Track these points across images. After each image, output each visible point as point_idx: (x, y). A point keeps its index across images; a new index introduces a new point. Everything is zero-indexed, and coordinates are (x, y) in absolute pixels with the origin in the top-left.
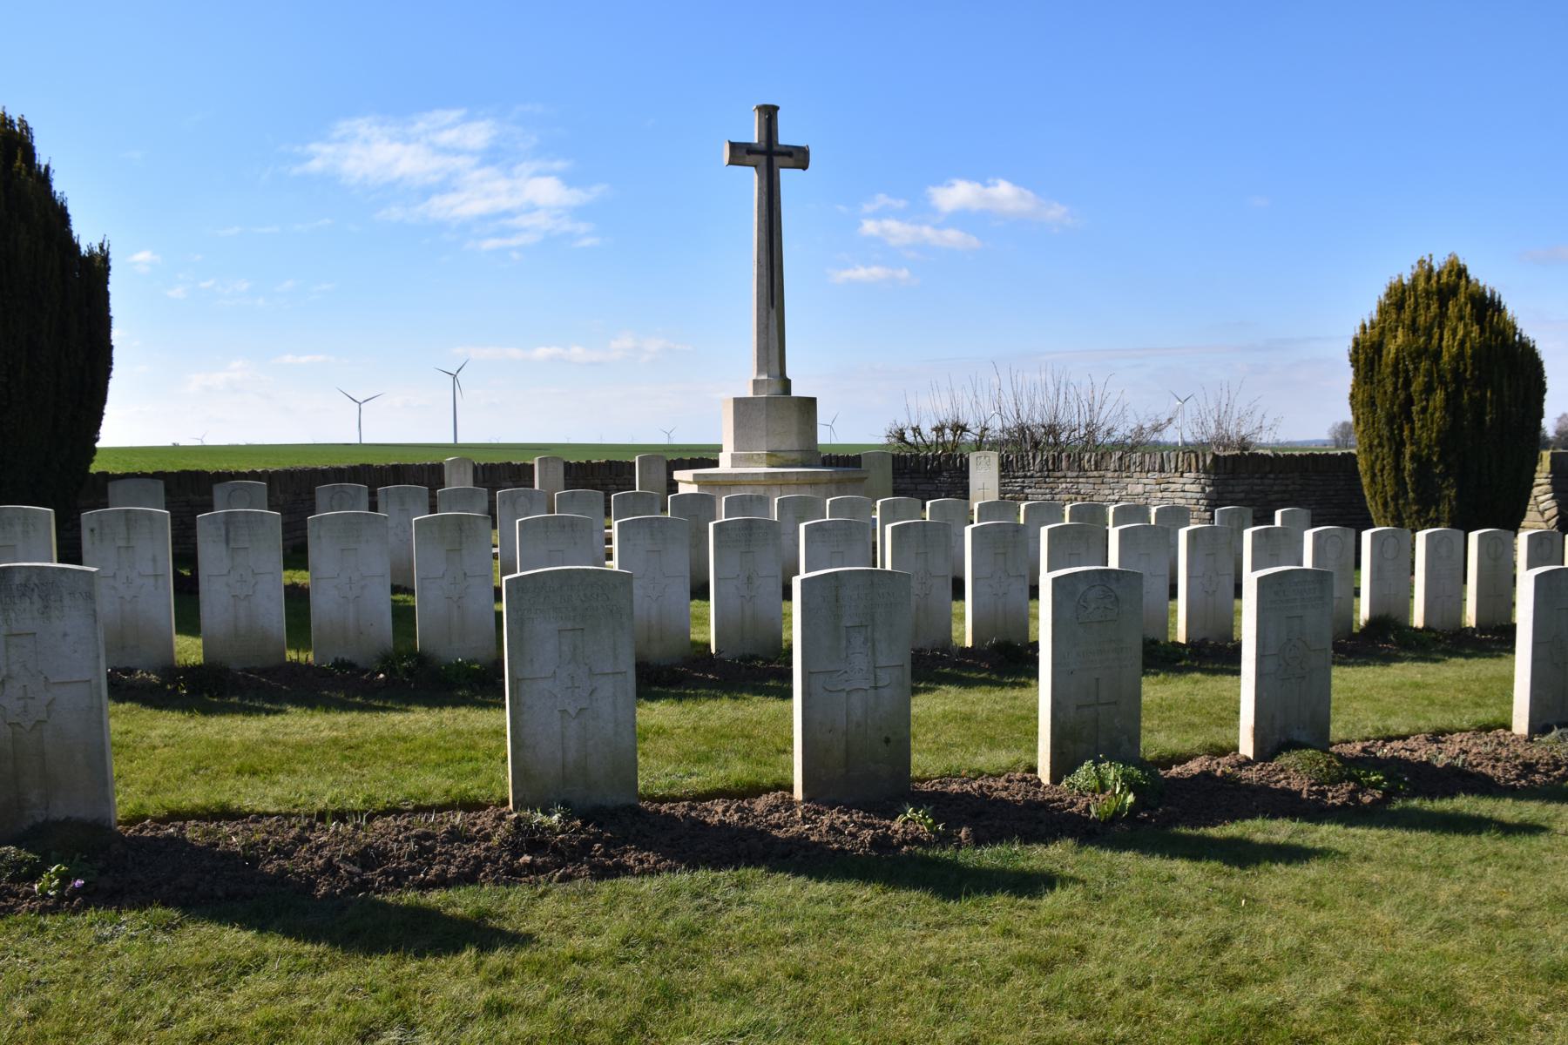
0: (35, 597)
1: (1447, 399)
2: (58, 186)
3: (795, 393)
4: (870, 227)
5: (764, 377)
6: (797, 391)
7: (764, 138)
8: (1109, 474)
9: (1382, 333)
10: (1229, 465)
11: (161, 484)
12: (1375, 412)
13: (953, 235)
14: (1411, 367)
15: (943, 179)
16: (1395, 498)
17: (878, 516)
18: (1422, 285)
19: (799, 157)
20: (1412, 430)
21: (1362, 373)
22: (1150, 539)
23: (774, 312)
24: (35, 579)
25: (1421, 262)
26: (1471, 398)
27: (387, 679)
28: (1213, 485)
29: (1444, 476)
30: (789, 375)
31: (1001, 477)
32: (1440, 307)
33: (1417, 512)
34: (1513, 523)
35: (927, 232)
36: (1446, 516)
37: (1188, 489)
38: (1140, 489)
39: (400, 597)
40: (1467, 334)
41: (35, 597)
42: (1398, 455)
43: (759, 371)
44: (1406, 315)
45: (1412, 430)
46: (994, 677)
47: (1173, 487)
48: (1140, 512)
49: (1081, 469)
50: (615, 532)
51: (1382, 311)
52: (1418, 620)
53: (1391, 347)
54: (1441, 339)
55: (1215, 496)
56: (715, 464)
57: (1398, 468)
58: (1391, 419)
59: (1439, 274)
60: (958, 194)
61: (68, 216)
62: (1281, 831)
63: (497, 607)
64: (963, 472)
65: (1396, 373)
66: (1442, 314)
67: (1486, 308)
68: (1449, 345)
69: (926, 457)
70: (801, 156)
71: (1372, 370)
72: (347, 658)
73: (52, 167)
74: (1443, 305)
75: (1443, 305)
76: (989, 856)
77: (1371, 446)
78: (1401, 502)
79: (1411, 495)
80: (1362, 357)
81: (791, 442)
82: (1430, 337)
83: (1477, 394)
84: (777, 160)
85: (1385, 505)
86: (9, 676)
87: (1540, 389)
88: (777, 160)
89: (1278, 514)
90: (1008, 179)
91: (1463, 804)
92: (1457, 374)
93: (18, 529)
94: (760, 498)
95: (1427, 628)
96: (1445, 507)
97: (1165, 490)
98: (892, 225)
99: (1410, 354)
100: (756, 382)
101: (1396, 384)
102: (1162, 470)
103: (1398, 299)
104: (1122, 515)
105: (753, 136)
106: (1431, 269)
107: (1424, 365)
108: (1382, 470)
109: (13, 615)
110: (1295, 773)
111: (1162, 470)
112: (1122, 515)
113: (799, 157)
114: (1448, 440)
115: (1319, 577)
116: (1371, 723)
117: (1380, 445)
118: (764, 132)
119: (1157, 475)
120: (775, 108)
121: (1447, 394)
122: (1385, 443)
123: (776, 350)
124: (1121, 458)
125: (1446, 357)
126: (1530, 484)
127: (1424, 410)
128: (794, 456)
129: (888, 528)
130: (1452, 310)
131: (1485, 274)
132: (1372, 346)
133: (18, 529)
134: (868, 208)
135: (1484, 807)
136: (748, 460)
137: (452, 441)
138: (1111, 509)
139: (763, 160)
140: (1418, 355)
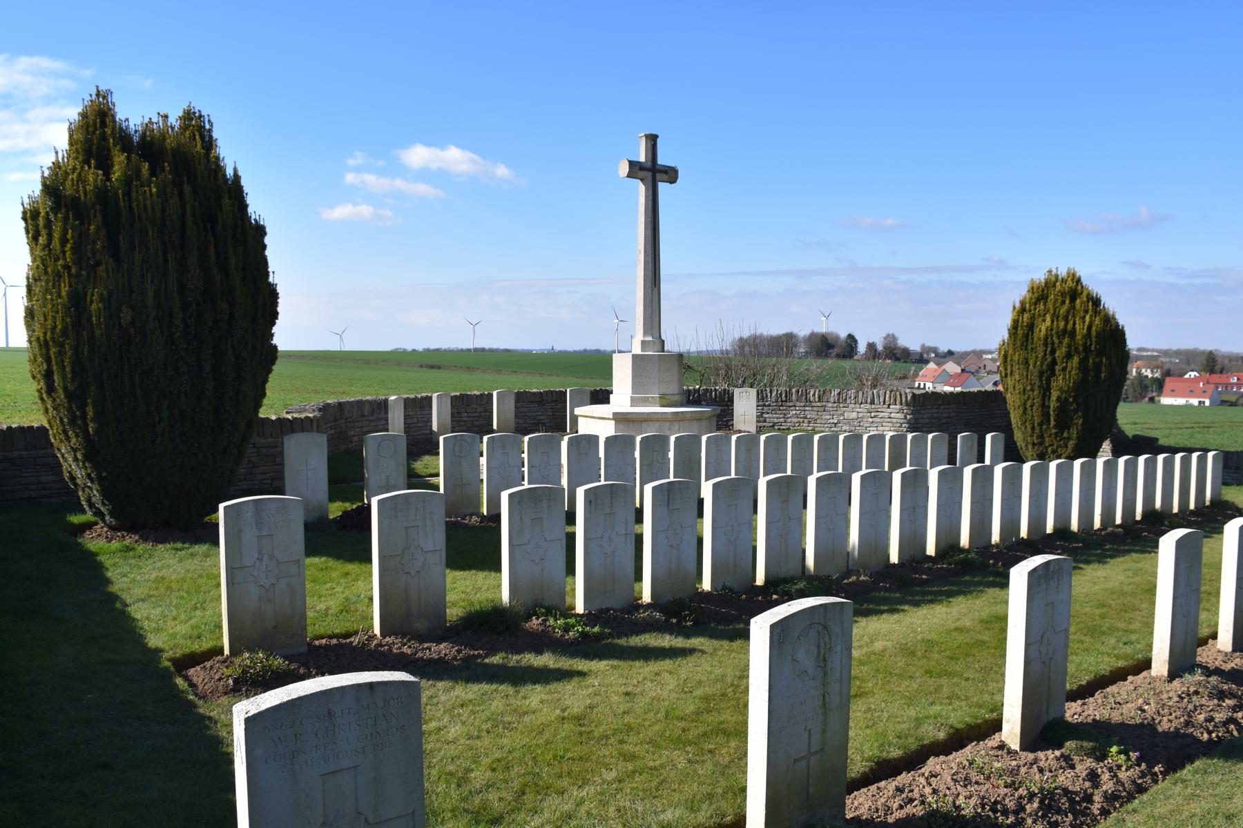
4: (350, 178)
5: (650, 339)
13: (422, 189)
15: (407, 143)
16: (1041, 425)
19: (671, 175)
21: (1019, 343)
23: (656, 290)
25: (1050, 272)
33: (1056, 434)
35: (399, 184)
38: (854, 415)
43: (645, 334)
53: (1043, 327)
54: (1074, 324)
57: (1044, 406)
58: (1041, 374)
60: (418, 155)
62: (546, 660)
63: (569, 529)
65: (1046, 345)
66: (1073, 307)
68: (1081, 329)
75: (1073, 300)
79: (1052, 423)
81: (673, 388)
84: (659, 176)
85: (1033, 428)
88: (659, 176)
90: (459, 145)
92: (1086, 348)
93: (545, 504)
98: (370, 178)
100: (643, 342)
102: (872, 402)
106: (1057, 276)
111: (872, 402)
113: (671, 175)
117: (1032, 390)
119: (868, 406)
122: (1036, 387)
125: (1078, 337)
127: (1064, 369)
131: (1092, 284)
133: (545, 504)
134: (351, 162)
136: (645, 402)
137: (4, 345)
139: (649, 175)
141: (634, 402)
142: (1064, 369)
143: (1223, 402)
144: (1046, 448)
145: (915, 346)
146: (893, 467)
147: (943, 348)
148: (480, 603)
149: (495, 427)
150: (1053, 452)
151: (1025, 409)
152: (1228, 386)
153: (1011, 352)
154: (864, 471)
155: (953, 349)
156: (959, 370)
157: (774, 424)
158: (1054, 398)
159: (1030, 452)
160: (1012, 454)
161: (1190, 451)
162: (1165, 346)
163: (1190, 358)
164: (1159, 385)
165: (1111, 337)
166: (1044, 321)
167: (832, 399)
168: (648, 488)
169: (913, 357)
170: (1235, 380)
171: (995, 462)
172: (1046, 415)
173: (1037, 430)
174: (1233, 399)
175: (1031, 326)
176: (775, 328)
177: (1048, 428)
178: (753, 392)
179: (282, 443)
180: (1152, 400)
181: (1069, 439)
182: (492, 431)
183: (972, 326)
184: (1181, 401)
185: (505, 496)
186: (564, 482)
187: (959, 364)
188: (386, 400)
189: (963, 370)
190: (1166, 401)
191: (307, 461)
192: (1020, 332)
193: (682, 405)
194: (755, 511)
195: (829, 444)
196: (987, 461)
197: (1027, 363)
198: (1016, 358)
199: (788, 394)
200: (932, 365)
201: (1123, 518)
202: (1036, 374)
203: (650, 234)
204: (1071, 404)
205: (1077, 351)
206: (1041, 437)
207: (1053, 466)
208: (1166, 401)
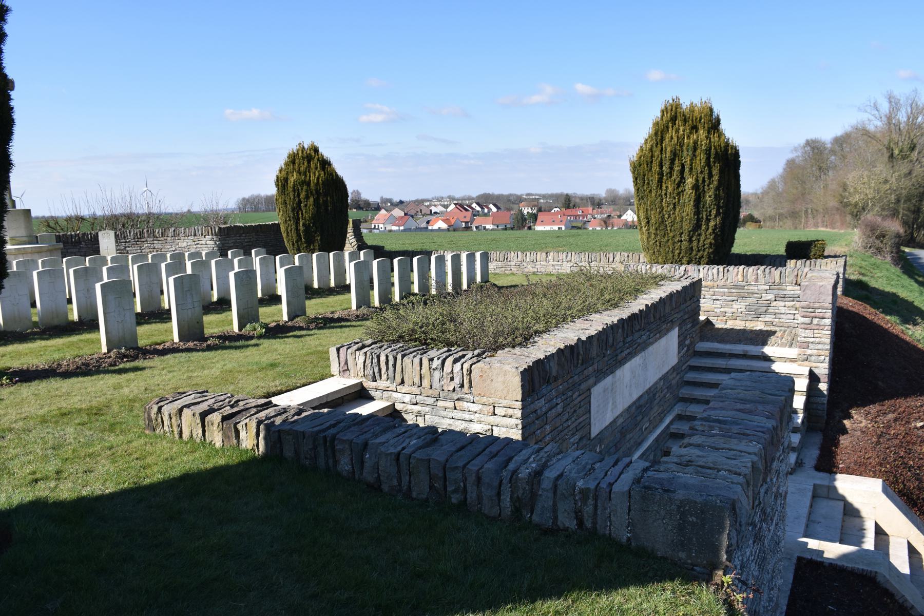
1: (314, 201)
9: (287, 174)
16: (297, 242)
17: (64, 266)
18: (300, 154)
22: (201, 265)
31: (116, 242)
34: (341, 248)
37: (207, 244)
38: (185, 244)
40: (319, 175)
42: (297, 224)
44: (296, 166)
48: (198, 254)
49: (154, 236)
50: (189, 265)
51: (287, 164)
52: (316, 286)
53: (292, 180)
57: (297, 230)
58: (293, 210)
65: (294, 191)
66: (309, 166)
67: (325, 164)
68: (313, 179)
74: (309, 162)
75: (309, 162)
76: (233, 344)
85: (293, 245)
87: (345, 186)
89: (229, 252)
91: (343, 324)
94: (33, 260)
95: (319, 288)
96: (317, 244)
102: (195, 235)
103: (293, 159)
104: (191, 256)
107: (305, 187)
110: (299, 321)
111: (195, 235)
112: (191, 256)
114: (315, 218)
115: (300, 267)
116: (314, 312)
125: (312, 185)
126: (346, 232)
127: (306, 206)
128: (25, 239)
129: (71, 271)
130: (312, 165)
131: (326, 152)
135: (349, 324)
138: (187, 254)
140: (303, 183)
143: (573, 227)
145: (374, 198)
147: (396, 199)
148: (906, 600)
152: (576, 216)
155: (403, 200)
156: (403, 214)
161: (391, 255)
162: (543, 192)
163: (556, 197)
164: (534, 217)
165: (336, 185)
170: (580, 213)
172: (298, 235)
174: (580, 225)
175: (286, 180)
178: (112, 233)
180: (530, 228)
183: (249, 179)
184: (548, 228)
187: (403, 210)
189: (406, 214)
190: (539, 228)
196: (230, 257)
199: (142, 233)
200: (383, 212)
208: (539, 228)
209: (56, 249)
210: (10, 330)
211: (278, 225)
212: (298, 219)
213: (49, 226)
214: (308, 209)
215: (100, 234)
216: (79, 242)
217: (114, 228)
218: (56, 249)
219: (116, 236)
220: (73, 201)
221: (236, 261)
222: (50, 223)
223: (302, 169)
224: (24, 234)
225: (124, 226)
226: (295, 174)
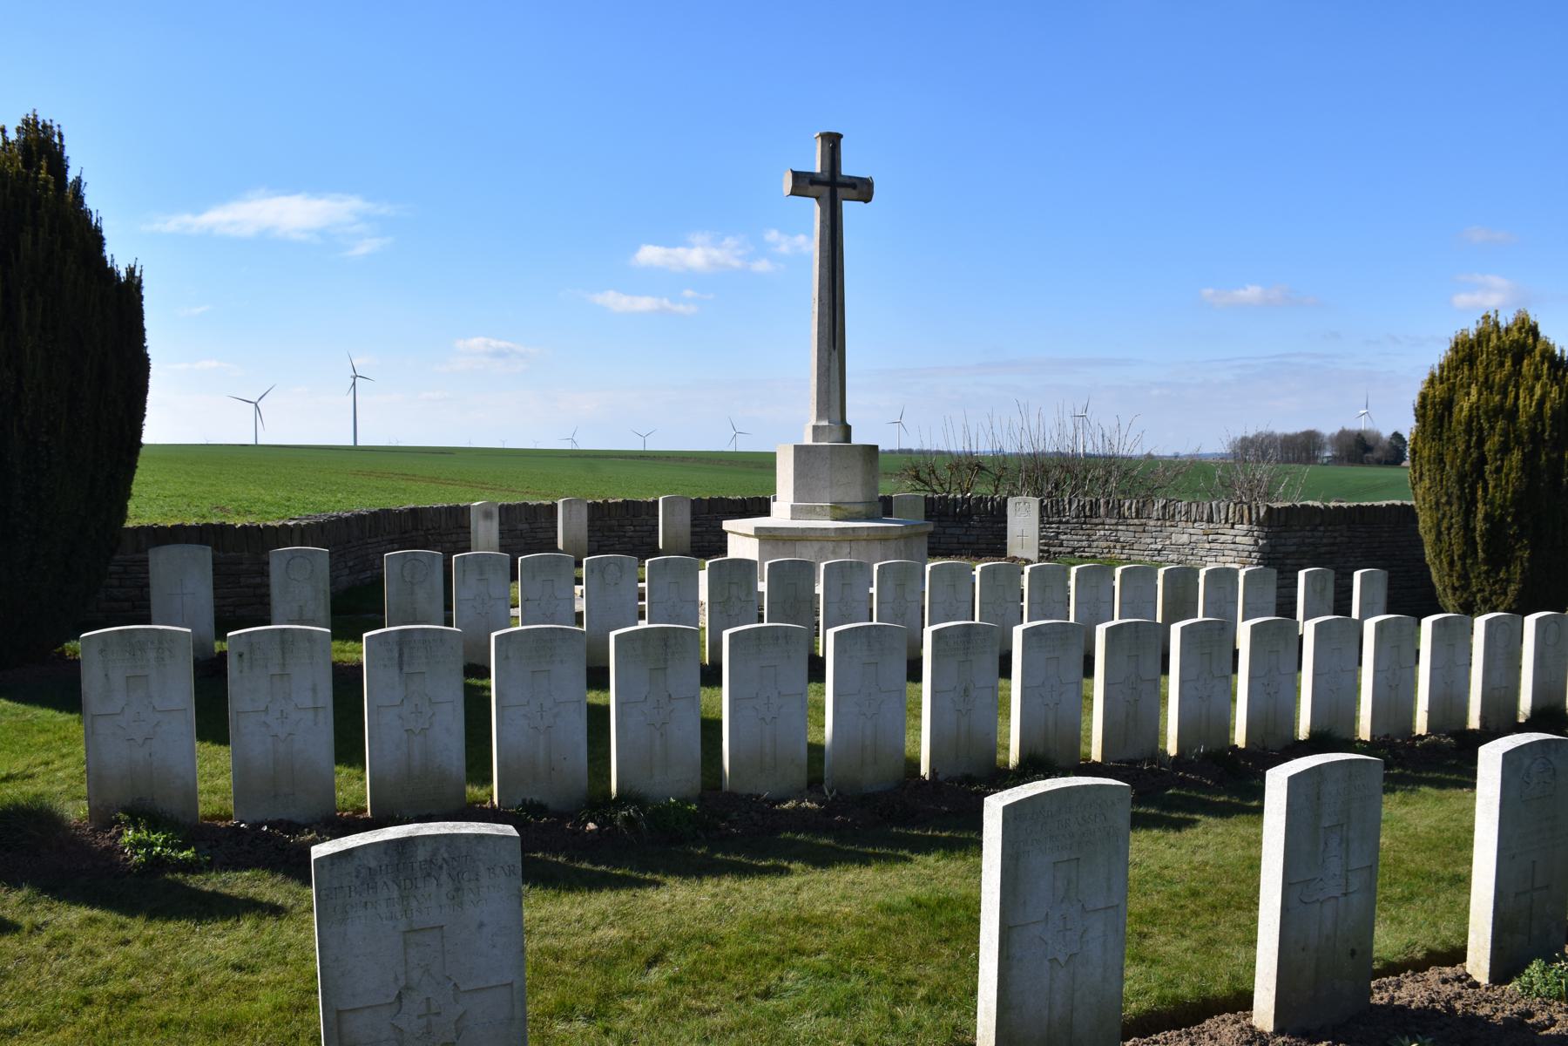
0: (444, 877)
1: (1525, 459)
2: (91, 201)
3: (857, 439)
5: (825, 423)
6: (857, 439)
7: (828, 168)
8: (1152, 523)
9: (1452, 389)
10: (1282, 518)
11: (205, 554)
12: (1443, 469)
14: (1486, 426)
16: (1463, 557)
19: (863, 189)
20: (1485, 490)
21: (1429, 429)
23: (835, 354)
24: (444, 853)
26: (1549, 460)
27: (600, 830)
28: (1266, 537)
29: (1518, 537)
30: (849, 421)
31: (1041, 521)
32: (1514, 365)
36: (1518, 577)
38: (1185, 538)
39: (473, 681)
41: (444, 877)
42: (1469, 512)
43: (819, 417)
45: (1485, 490)
46: (1236, 800)
47: (1223, 538)
49: (1121, 516)
54: (1517, 398)
55: (1268, 549)
56: (767, 513)
57: (1468, 529)
58: (1462, 478)
59: (1507, 330)
61: (102, 239)
63: (594, 697)
64: (998, 517)
65: (1469, 431)
66: (1517, 372)
68: (1526, 405)
69: (955, 499)
70: (865, 188)
71: (1441, 426)
72: (536, 798)
73: (84, 179)
75: (1517, 361)
77: (1437, 503)
78: (1469, 561)
79: (1481, 554)
80: (1430, 413)
81: (854, 494)
82: (1505, 395)
83: (1555, 455)
84: (841, 192)
85: (1451, 563)
86: (408, 988)
88: (841, 192)
92: (1535, 436)
93: (152, 655)
94: (860, 565)
97: (1214, 541)
99: (1486, 413)
100: (815, 428)
101: (1468, 442)
102: (1210, 520)
103: (1467, 353)
105: (816, 166)
106: (1497, 324)
107: (1500, 425)
108: (1449, 529)
109: (414, 904)
111: (1210, 520)
113: (863, 189)
117: (1449, 503)
118: (827, 161)
119: (1204, 525)
120: (839, 136)
121: (1524, 454)
122: (1454, 500)
123: (838, 394)
124: (1164, 507)
125: (1523, 419)
127: (1498, 470)
128: (859, 508)
132: (1441, 403)
133: (152, 655)
136: (810, 513)
137: (352, 443)
139: (826, 191)
140: (1499, 411)
141: (796, 512)
142: (1498, 470)
144: (1474, 594)
146: (1170, 618)
149: (560, 546)
150: (1485, 601)
151: (1439, 533)
153: (1420, 444)
154: (1026, 624)
157: (1074, 550)
158: (1480, 516)
159: (1450, 601)
160: (1410, 598)
166: (1468, 394)
167: (1155, 515)
168: (831, 633)
169: (1377, 454)
171: (1366, 612)
172: (1469, 541)
173: (1458, 566)
175: (1448, 404)
176: (1288, 422)
177: (1475, 563)
178: (1034, 503)
179: (147, 560)
181: (1508, 581)
182: (657, 552)
185: (726, 634)
186: (704, 620)
188: (468, 508)
191: (185, 583)
192: (1430, 413)
193: (868, 519)
194: (1235, 670)
195: (1140, 577)
196: (1355, 614)
197: (1440, 460)
198: (1426, 453)
199: (1094, 506)
201: (1483, 718)
202: (1454, 478)
203: (827, 275)
204: (1510, 526)
205: (1519, 441)
206: (1464, 576)
207: (1480, 623)
209: (918, 535)
210: (746, 790)
211: (1408, 514)
212: (1474, 502)
213: (917, 477)
214: (1506, 476)
215: (1011, 502)
216: (968, 515)
217: (1037, 492)
218: (918, 535)
219: (1043, 508)
220: (966, 428)
221: (1370, 626)
222: (920, 466)
223: (1498, 378)
224: (860, 499)
225: (1056, 487)
226: (1474, 390)
